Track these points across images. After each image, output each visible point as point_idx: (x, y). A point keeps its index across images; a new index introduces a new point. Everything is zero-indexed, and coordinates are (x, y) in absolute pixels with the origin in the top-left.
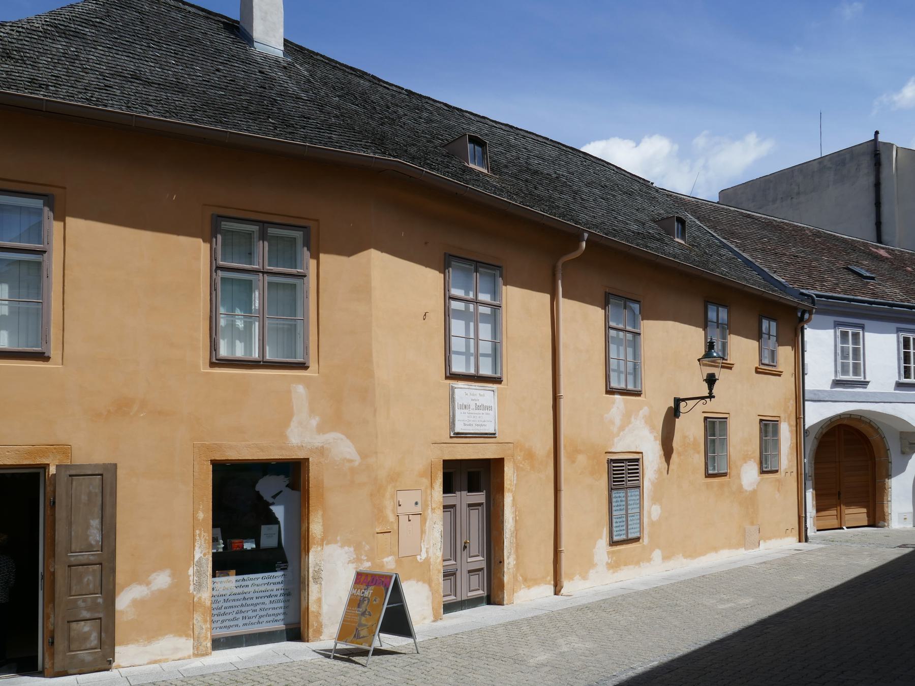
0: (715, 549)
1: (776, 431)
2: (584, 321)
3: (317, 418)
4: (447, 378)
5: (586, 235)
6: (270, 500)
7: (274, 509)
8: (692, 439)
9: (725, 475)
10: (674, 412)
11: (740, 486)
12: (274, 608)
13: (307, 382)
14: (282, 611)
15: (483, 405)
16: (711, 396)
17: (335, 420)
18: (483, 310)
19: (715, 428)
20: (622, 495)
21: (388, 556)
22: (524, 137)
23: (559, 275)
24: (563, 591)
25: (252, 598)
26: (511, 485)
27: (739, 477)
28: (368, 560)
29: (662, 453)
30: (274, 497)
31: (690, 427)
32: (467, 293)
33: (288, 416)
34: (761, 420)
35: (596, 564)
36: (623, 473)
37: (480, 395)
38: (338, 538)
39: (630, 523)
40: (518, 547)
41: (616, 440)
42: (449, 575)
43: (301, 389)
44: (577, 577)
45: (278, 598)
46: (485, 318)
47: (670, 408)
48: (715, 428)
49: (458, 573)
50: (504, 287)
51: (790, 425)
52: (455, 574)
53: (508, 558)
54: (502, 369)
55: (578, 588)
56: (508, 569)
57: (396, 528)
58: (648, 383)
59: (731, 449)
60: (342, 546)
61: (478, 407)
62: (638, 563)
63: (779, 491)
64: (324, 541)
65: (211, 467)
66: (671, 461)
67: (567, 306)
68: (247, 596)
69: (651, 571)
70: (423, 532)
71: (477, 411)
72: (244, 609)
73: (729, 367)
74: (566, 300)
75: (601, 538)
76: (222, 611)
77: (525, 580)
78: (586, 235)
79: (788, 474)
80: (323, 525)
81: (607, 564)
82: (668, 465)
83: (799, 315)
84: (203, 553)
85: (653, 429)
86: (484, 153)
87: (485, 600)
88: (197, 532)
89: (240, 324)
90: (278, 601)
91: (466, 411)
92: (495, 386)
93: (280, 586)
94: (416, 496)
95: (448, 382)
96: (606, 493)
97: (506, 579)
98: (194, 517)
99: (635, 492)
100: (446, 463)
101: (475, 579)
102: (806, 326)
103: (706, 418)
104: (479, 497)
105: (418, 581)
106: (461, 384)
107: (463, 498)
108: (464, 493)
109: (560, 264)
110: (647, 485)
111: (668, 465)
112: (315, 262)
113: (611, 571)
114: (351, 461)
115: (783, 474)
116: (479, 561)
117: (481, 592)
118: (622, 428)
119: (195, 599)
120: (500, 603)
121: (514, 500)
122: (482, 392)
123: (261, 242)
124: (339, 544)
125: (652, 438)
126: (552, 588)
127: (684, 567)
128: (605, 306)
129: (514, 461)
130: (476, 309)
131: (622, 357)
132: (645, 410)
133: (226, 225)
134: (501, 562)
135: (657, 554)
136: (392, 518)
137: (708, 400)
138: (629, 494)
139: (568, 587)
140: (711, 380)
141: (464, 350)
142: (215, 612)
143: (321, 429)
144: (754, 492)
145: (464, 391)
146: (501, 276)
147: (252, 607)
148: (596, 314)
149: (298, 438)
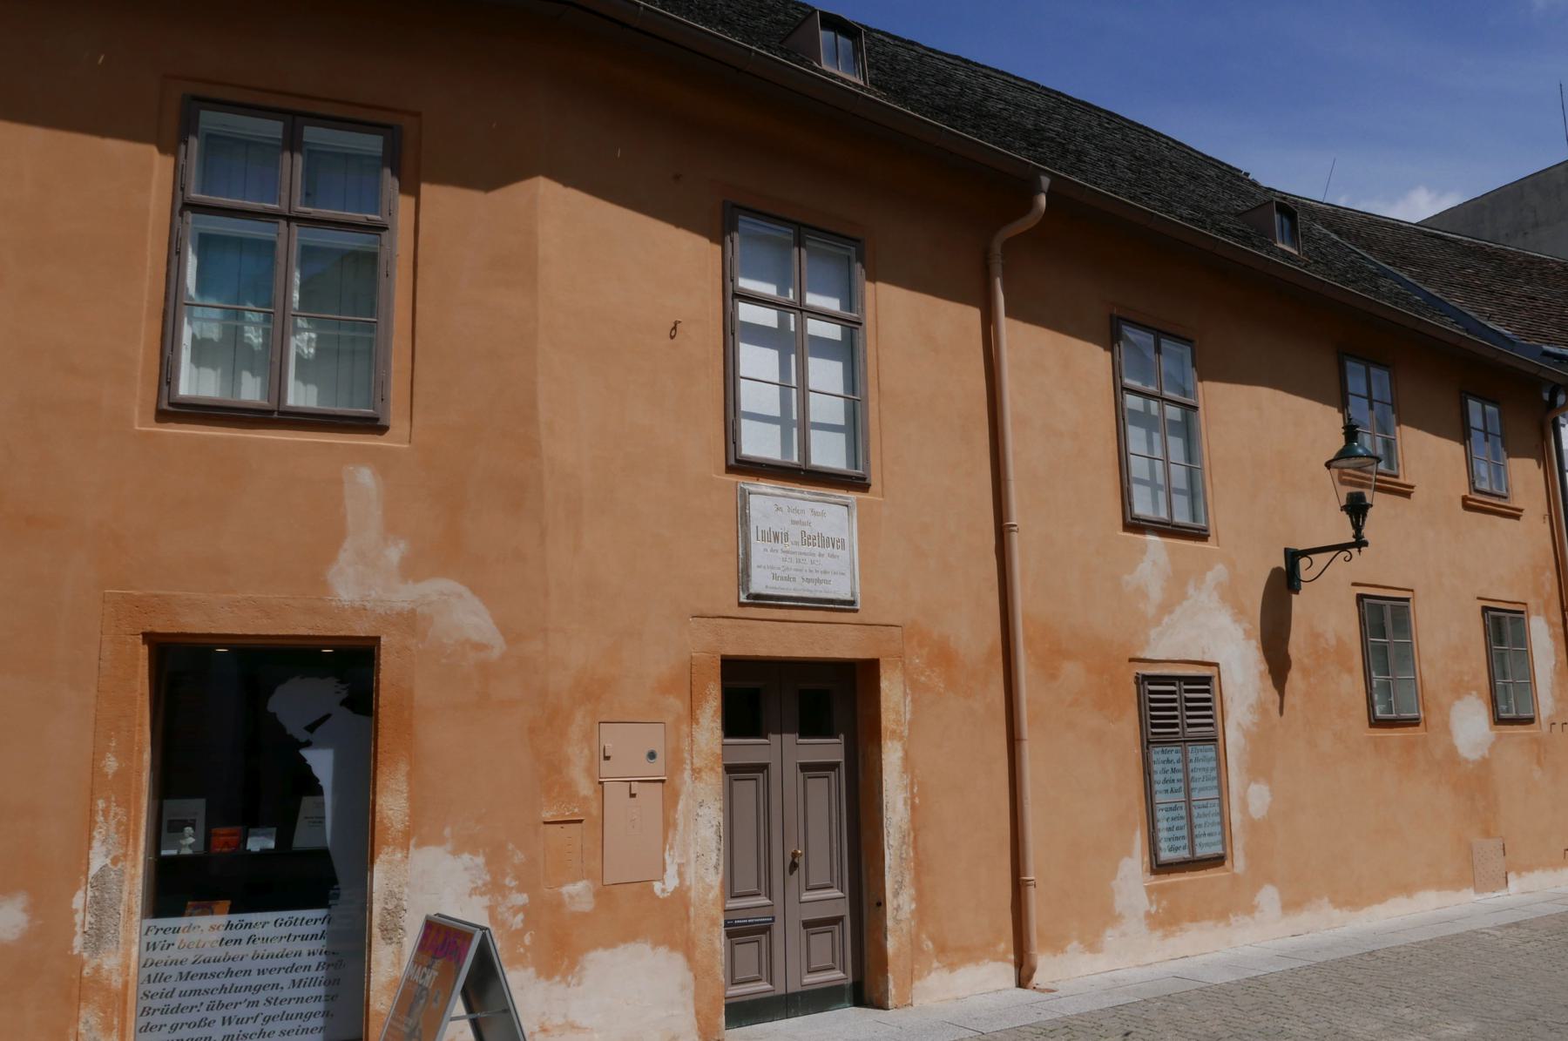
0: (1408, 889)
1: (1522, 639)
2: (1061, 378)
3: (403, 545)
4: (730, 469)
5: (1045, 181)
6: (303, 736)
7: (309, 755)
8: (1333, 642)
9: (1414, 722)
10: (1286, 580)
11: (1452, 754)
12: (300, 1000)
13: (383, 464)
14: (319, 1007)
15: (820, 535)
16: (1360, 543)
17: (443, 552)
18: (815, 327)
19: (1384, 618)
20: (1175, 756)
21: (575, 880)
22: (987, 77)
23: (997, 267)
24: (1037, 978)
25: (248, 972)
26: (898, 722)
27: (1446, 729)
28: (520, 890)
29: (1264, 667)
30: (311, 728)
31: (1325, 613)
32: (782, 290)
33: (331, 537)
34: (1485, 609)
35: (1120, 916)
36: (1175, 707)
37: (815, 513)
38: (447, 832)
39: (1196, 821)
40: (920, 868)
41: (1153, 633)
42: (737, 931)
43: (365, 476)
44: (1074, 944)
45: (312, 974)
46: (824, 348)
47: (1276, 572)
48: (1384, 618)
49: (777, 928)
50: (869, 286)
51: (1550, 624)
52: (766, 929)
53: (896, 894)
54: (867, 459)
55: (1075, 974)
56: (898, 922)
57: (595, 811)
58: (1221, 515)
59: (1424, 667)
60: (456, 852)
61: (807, 540)
62: (1223, 915)
63: (1539, 763)
64: (416, 833)
65: (144, 651)
66: (1287, 686)
67: (1012, 332)
68: (235, 967)
69: (1255, 936)
70: (668, 824)
71: (805, 549)
72: (227, 998)
73: (1405, 492)
74: (1011, 321)
75: (1130, 855)
76: (174, 1001)
77: (942, 949)
78: (1045, 181)
79: (1558, 727)
80: (411, 799)
81: (1148, 915)
82: (1282, 694)
83: (1546, 396)
84: (118, 859)
85: (1239, 612)
86: (857, 49)
87: (848, 995)
88: (101, 804)
89: (254, 336)
90: (312, 982)
91: (779, 546)
92: (852, 497)
93: (319, 945)
94: (653, 737)
95: (733, 478)
96: (1137, 751)
97: (891, 945)
98: (96, 770)
99: (1208, 751)
100: (733, 668)
101: (822, 943)
102: (1562, 420)
103: (1360, 597)
104: (830, 749)
105: (656, 944)
106: (765, 486)
107: (785, 751)
108: (790, 739)
109: (997, 247)
110: (1234, 738)
111: (1282, 694)
112: (411, 201)
113: (1159, 933)
114: (479, 647)
115: (1546, 728)
116: (833, 899)
117: (837, 975)
118: (1166, 608)
119: (87, 971)
120: (881, 1005)
121: (906, 758)
122: (818, 507)
123: (287, 155)
124: (449, 847)
125: (1240, 634)
126: (1011, 970)
127: (1333, 928)
128: (1111, 340)
129: (905, 671)
130: (802, 326)
131: (1158, 453)
132: (1218, 573)
133: (210, 120)
134: (881, 904)
135: (1269, 897)
136: (585, 787)
137: (1354, 551)
138: (1191, 756)
139: (1046, 968)
140: (1356, 509)
141: (777, 413)
142: (157, 1003)
143: (410, 570)
144: (1485, 763)
145: (769, 503)
146: (860, 259)
147: (248, 996)
148: (1093, 360)
149: (360, 583)
